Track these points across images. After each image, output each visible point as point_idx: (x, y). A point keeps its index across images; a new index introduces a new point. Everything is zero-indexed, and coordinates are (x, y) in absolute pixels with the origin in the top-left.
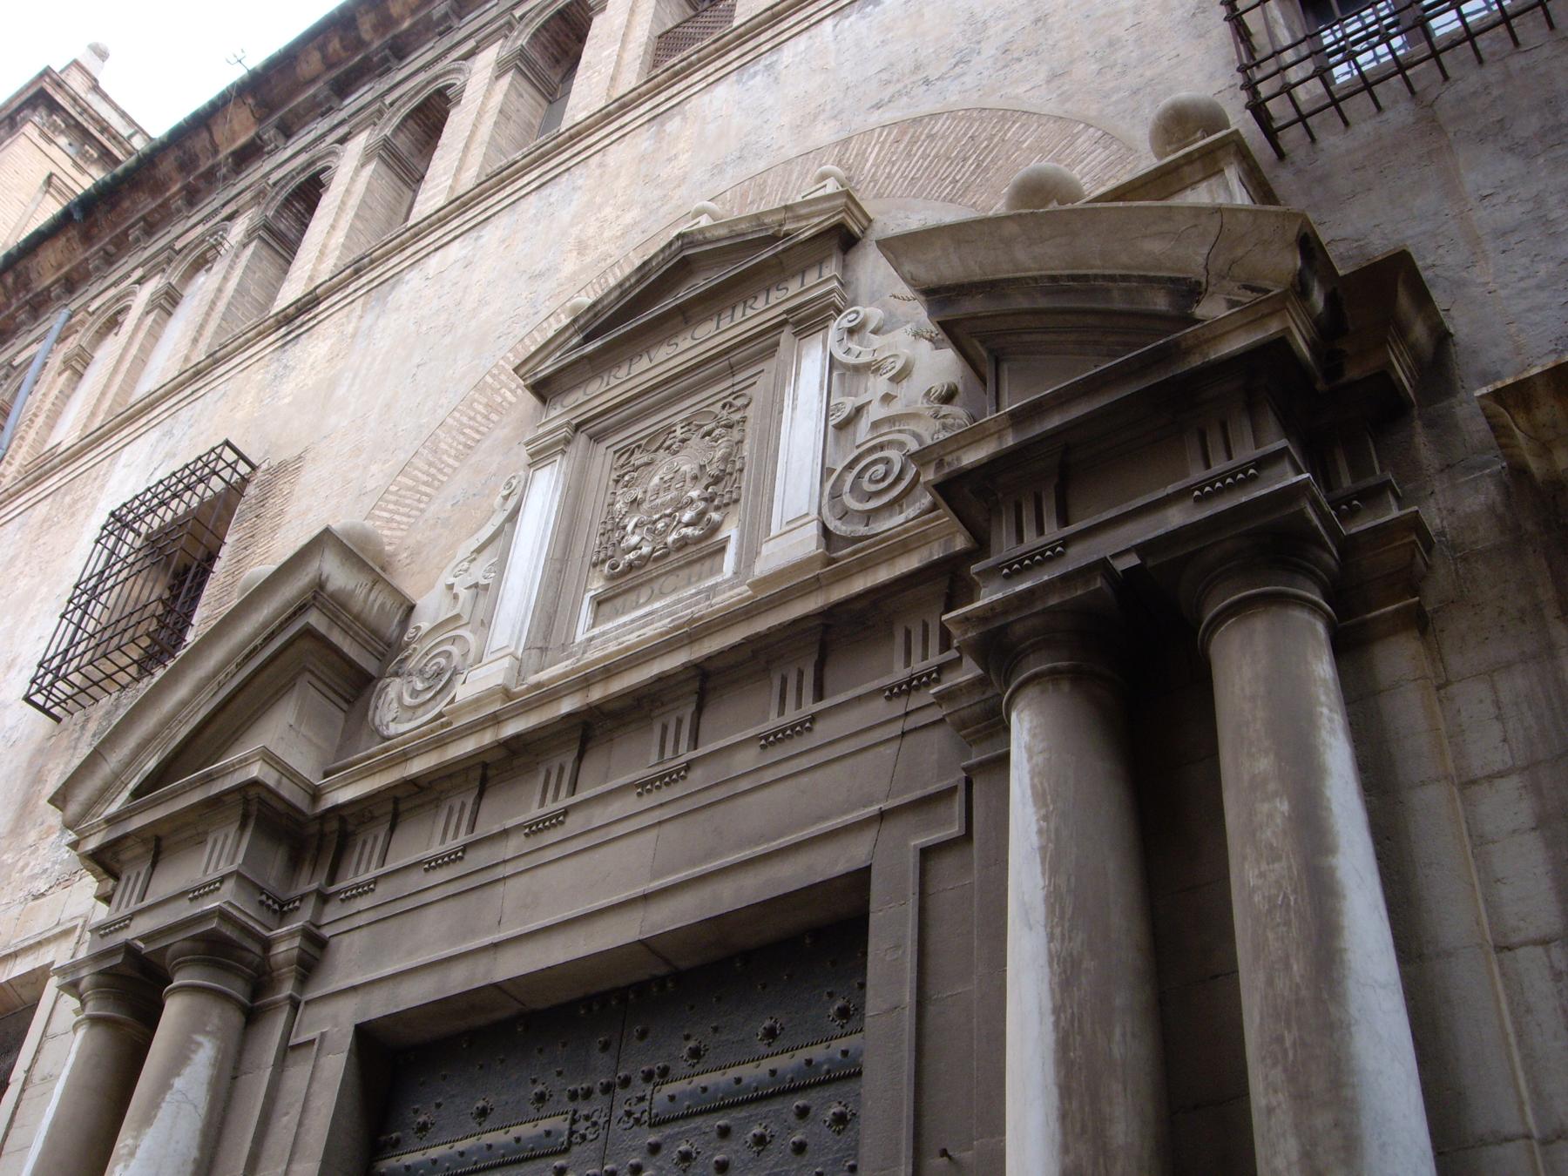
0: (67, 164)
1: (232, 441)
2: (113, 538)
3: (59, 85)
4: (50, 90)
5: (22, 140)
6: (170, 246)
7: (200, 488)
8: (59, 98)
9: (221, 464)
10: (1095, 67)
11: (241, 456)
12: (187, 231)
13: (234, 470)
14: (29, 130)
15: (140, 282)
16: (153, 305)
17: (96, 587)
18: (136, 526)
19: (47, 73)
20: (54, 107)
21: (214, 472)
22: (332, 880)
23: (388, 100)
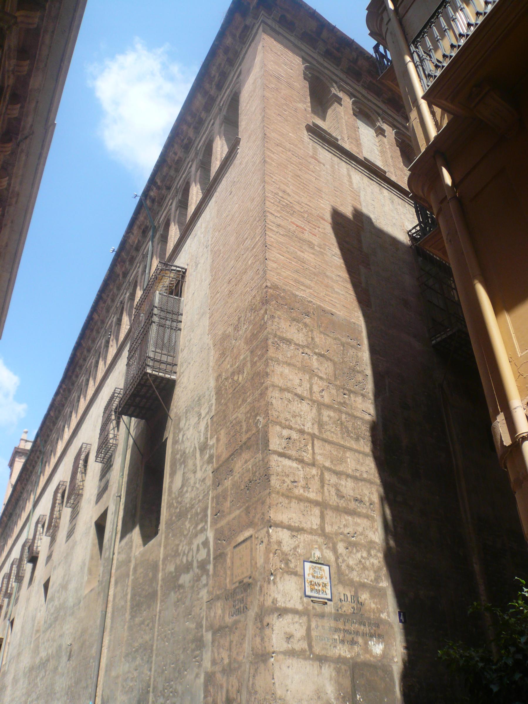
8: (19, 451)
14: (17, 459)
20: (19, 452)
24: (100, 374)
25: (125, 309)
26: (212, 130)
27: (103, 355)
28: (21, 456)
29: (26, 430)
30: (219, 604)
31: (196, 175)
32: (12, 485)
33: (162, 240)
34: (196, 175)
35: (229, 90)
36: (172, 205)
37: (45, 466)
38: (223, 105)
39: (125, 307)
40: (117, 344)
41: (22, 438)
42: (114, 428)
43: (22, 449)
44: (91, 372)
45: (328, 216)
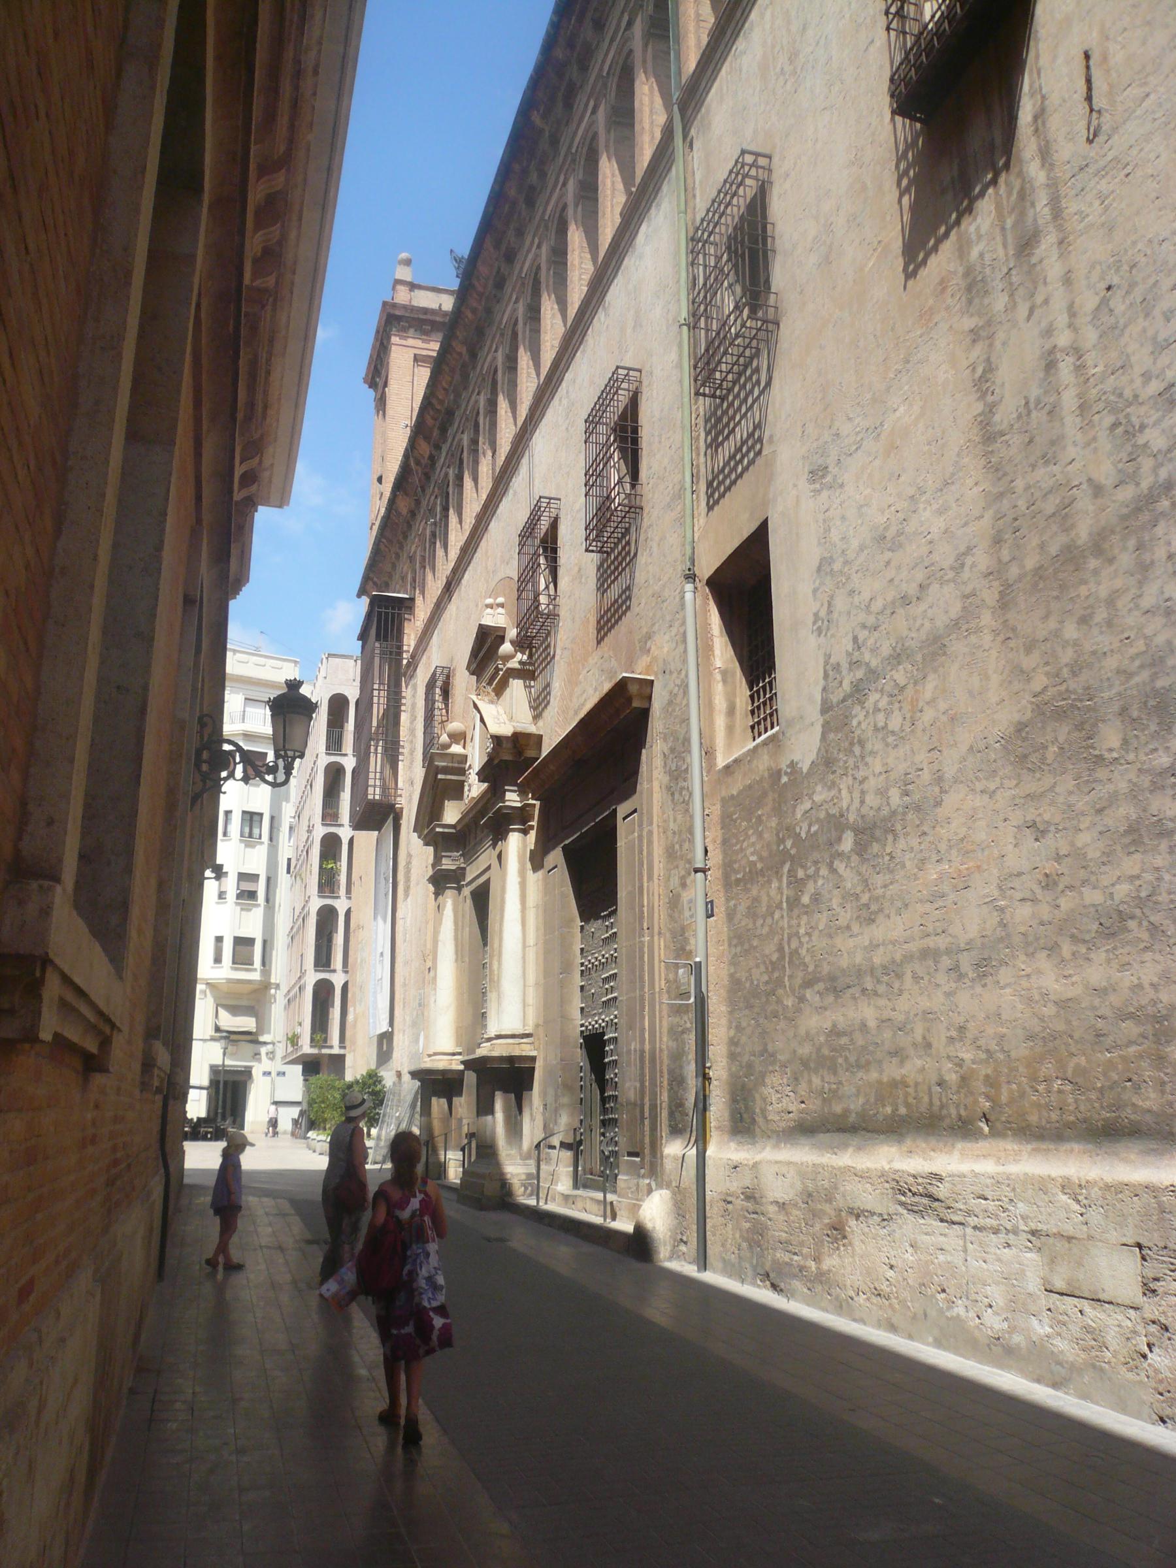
0: (419, 343)
1: (745, 147)
2: (701, 256)
3: (394, 306)
4: (392, 312)
5: (394, 348)
6: (599, 75)
7: (741, 191)
8: (397, 313)
9: (747, 168)
10: (829, 577)
11: (757, 155)
12: (605, 59)
13: (758, 167)
14: (395, 339)
15: (594, 112)
16: (648, 36)
17: (705, 297)
18: (712, 239)
19: (385, 304)
20: (399, 318)
21: (746, 176)
22: (887, 778)
23: (573, 151)
24: (506, 431)
25: (543, 286)
26: (593, 122)
27: (524, 338)
28: (404, 330)
29: (404, 255)
30: (1148, 562)
31: (524, 332)
32: (458, 260)
33: (555, 262)
34: (524, 332)
35: (615, 44)
36: (595, 117)
37: (446, 517)
38: (608, 73)
39: (543, 279)
40: (538, 375)
41: (398, 277)
42: (547, 587)
43: (405, 307)
44: (449, 499)
45: (985, 219)
